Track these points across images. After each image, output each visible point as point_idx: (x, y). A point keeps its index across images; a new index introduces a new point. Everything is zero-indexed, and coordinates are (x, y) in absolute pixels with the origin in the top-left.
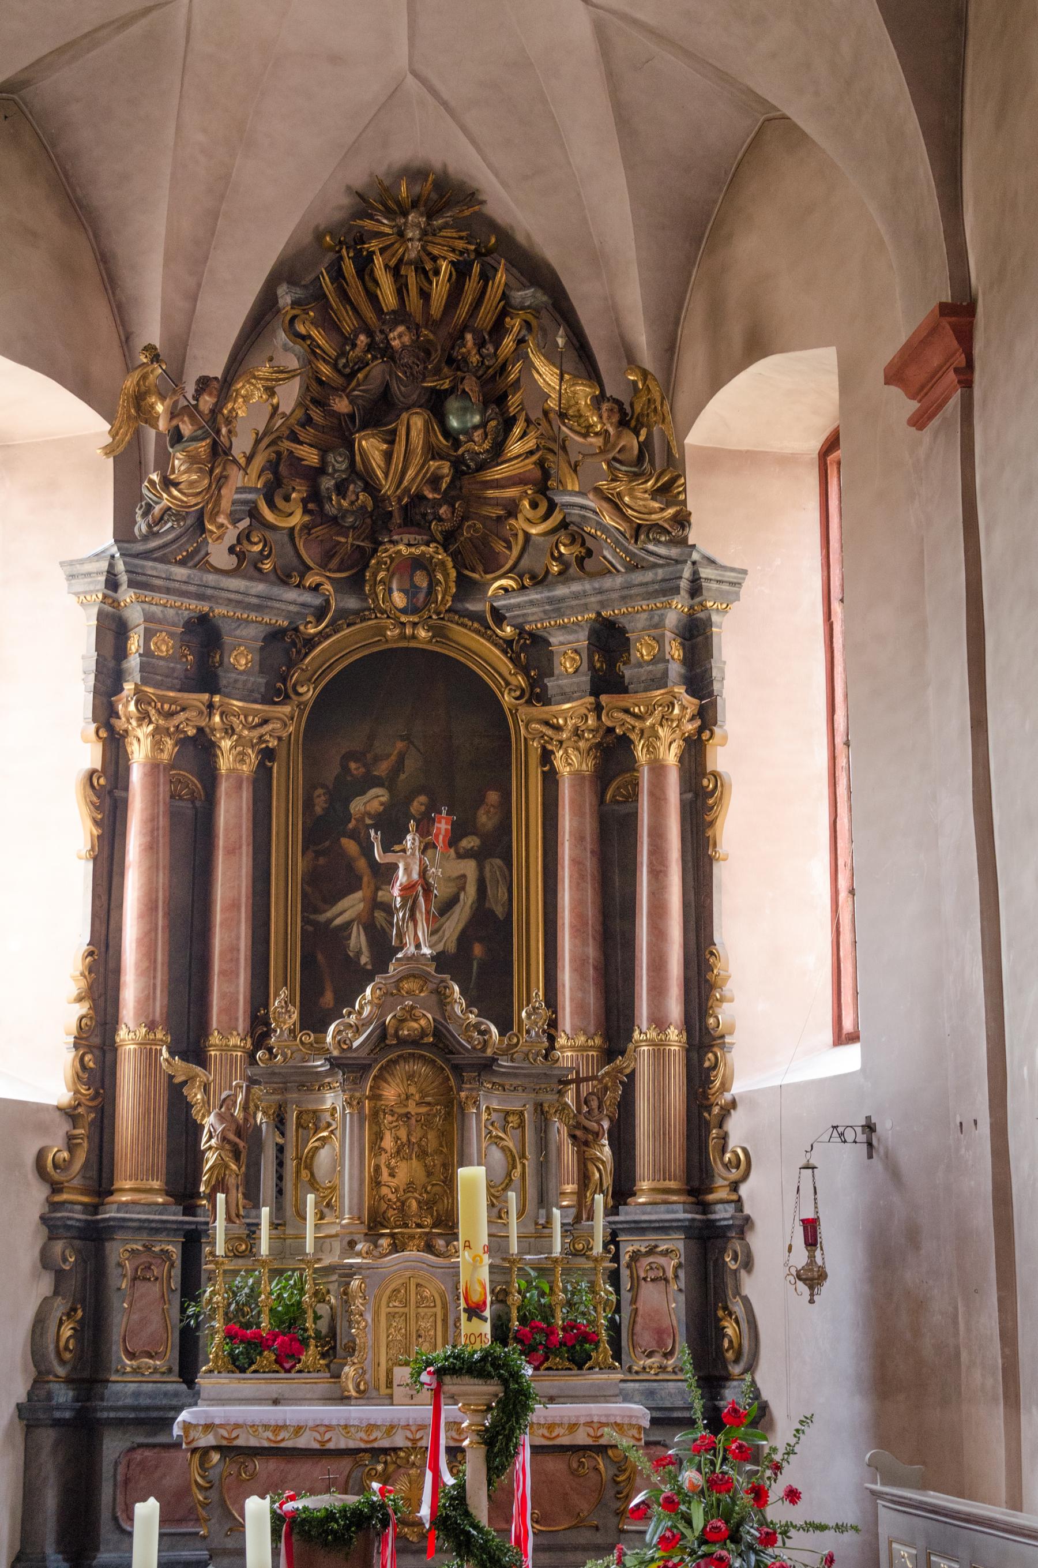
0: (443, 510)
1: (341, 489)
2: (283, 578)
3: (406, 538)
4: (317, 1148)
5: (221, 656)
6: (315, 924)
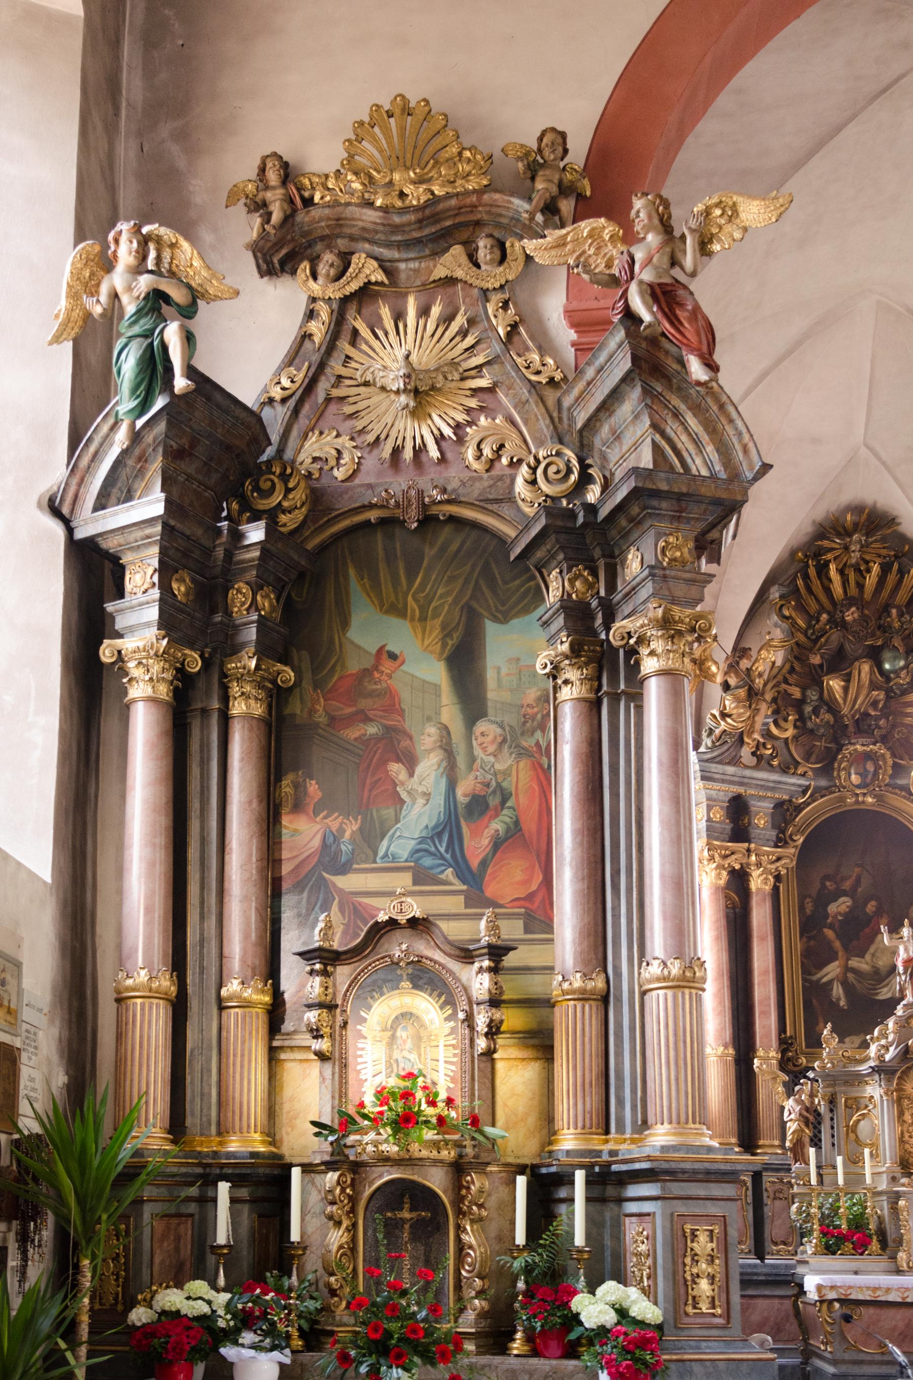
0: (882, 722)
1: (816, 711)
2: (784, 769)
3: (861, 740)
4: (858, 1121)
5: (749, 820)
6: (811, 982)
